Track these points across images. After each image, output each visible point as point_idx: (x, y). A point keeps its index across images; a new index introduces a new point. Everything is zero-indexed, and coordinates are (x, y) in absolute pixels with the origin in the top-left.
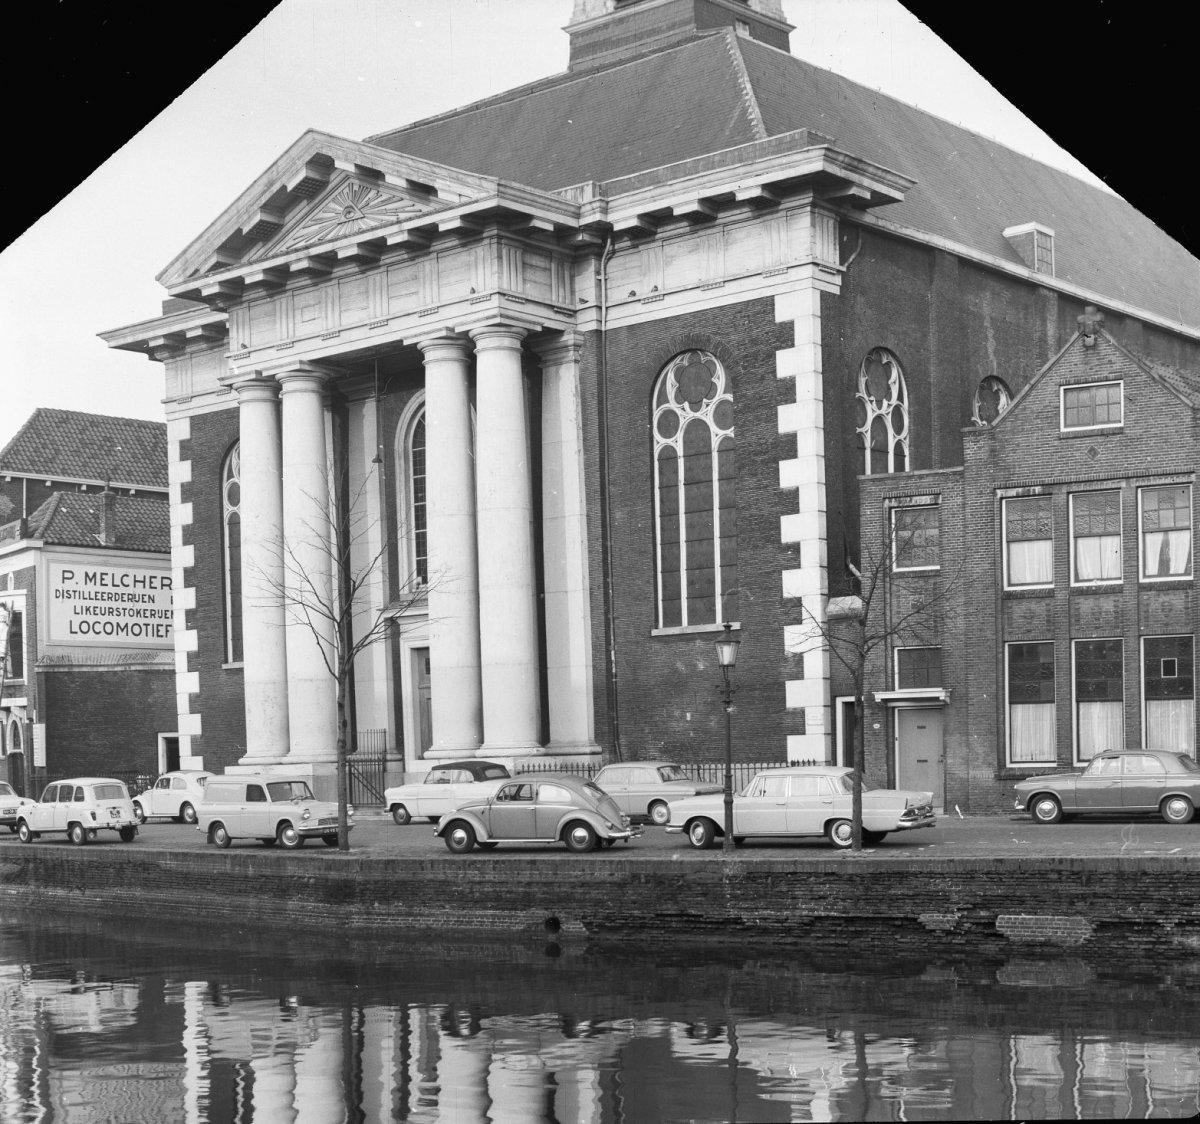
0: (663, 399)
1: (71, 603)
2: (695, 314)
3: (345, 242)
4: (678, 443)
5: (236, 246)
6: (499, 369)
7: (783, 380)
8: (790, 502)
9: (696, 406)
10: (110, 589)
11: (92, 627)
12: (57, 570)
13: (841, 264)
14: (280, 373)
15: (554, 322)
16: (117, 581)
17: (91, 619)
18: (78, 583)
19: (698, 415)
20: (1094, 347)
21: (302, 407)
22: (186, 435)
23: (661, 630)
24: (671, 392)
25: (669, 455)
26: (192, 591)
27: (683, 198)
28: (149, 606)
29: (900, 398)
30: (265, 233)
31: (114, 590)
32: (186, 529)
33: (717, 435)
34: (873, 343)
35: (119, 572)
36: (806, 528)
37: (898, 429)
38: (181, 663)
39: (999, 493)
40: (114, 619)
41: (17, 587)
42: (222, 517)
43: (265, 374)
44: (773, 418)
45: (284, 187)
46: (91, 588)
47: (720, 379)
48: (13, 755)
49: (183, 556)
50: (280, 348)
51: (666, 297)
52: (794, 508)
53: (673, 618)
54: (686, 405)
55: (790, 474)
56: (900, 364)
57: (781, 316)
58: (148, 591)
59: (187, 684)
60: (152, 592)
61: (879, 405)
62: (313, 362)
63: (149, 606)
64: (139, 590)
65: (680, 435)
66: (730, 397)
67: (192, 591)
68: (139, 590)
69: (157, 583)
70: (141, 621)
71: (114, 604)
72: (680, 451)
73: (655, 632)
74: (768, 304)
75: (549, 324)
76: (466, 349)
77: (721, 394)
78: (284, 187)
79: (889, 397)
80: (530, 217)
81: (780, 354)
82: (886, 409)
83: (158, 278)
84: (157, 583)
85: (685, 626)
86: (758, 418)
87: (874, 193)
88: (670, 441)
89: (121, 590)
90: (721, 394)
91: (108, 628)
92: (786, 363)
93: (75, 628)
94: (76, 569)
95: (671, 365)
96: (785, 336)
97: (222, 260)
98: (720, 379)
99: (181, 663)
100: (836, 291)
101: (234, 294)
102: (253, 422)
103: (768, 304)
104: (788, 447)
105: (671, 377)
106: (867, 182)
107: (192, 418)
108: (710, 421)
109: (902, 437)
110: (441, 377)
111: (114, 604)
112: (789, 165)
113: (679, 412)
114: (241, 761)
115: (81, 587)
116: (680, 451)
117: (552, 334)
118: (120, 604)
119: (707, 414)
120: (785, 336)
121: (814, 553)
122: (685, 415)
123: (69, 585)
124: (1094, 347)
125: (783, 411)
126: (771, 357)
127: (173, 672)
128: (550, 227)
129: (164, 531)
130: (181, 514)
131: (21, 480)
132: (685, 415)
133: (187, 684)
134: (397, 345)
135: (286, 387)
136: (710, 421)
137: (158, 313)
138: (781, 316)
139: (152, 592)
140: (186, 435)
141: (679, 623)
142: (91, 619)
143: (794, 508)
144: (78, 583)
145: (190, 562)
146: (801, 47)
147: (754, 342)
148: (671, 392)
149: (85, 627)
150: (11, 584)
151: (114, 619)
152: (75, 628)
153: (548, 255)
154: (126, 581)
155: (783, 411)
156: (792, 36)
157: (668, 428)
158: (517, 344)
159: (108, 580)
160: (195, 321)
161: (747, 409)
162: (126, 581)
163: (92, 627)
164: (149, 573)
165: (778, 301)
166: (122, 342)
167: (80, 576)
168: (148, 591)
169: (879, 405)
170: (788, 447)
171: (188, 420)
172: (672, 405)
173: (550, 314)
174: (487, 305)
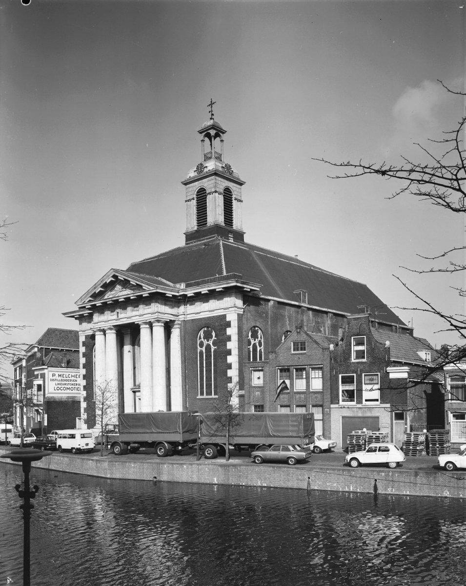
0: (200, 338)
1: (55, 382)
2: (208, 317)
3: (121, 297)
4: (204, 349)
5: (95, 296)
6: (159, 331)
7: (228, 335)
8: (230, 366)
9: (208, 341)
10: (65, 378)
11: (60, 389)
12: (51, 374)
13: (243, 306)
14: (105, 328)
15: (173, 318)
16: (67, 376)
17: (60, 386)
18: (57, 377)
19: (208, 343)
20: (299, 332)
21: (112, 336)
22: (84, 340)
23: (199, 397)
24: (202, 337)
25: (201, 353)
26: (85, 380)
27: (204, 290)
28: (76, 383)
29: (261, 338)
30: (101, 294)
31: (66, 379)
32: (83, 364)
33: (213, 348)
34: (253, 324)
35: (67, 374)
36: (233, 373)
37: (260, 346)
38: (82, 400)
39: (277, 368)
40: (66, 386)
41: (41, 378)
42: (11, 464)
43: (102, 328)
44: (226, 345)
45: (106, 282)
46: (60, 378)
47: (214, 334)
48: (39, 421)
49: (83, 371)
50: (105, 322)
51: (367, 166)
52: (230, 368)
53: (202, 394)
54: (206, 340)
55: (230, 359)
56: (261, 330)
57: (228, 319)
58: (75, 379)
59: (83, 405)
60: (76, 379)
61: (255, 341)
62: (113, 326)
63: (76, 383)
64: (73, 378)
65: (204, 348)
66: (216, 338)
67: (85, 380)
68: (73, 378)
69: (78, 376)
70: (73, 386)
71: (66, 382)
72: (204, 352)
73: (197, 397)
74: (224, 316)
75: (171, 319)
76: (151, 325)
77: (214, 338)
78: (106, 282)
79: (258, 338)
80: (166, 294)
81: (227, 329)
82: (257, 341)
83: (75, 303)
84: (78, 376)
85: (205, 396)
86: (222, 345)
87: (251, 289)
88: (202, 349)
89: (68, 378)
90: (214, 338)
91: (64, 389)
92: (229, 331)
93: (56, 389)
94: (57, 374)
95: (203, 329)
96: (228, 324)
97: (91, 299)
98: (214, 334)
99: (82, 400)
100: (242, 313)
101: (94, 308)
102: (99, 338)
103: (224, 316)
104: (229, 353)
105: (202, 333)
106: (248, 287)
107: (86, 336)
108: (211, 344)
109: (261, 348)
110: (144, 332)
111: (66, 382)
112: (228, 283)
113: (204, 342)
114: (94, 427)
115: (57, 378)
116: (204, 352)
117: (172, 322)
118: (68, 382)
119: (211, 342)
120: (228, 324)
121: (235, 379)
122: (205, 342)
123: (54, 378)
124: (299, 332)
125: (228, 343)
126: (225, 330)
127: (80, 402)
128: (171, 296)
129: (79, 364)
130: (83, 360)
131: (43, 348)
132: (205, 342)
133: (83, 405)
134: (133, 323)
135: (107, 332)
136: (211, 344)
137: (77, 309)
138: (228, 319)
139: (76, 379)
140: (84, 340)
141: (211, 395)
142: (60, 386)
143: (230, 368)
144: (57, 377)
145: (85, 373)
146: (247, 239)
147: (221, 325)
148: (202, 337)
149: (58, 389)
150: (39, 377)
151: (66, 386)
152: (56, 389)
153: (172, 301)
154: (69, 376)
155: (228, 343)
156: (245, 235)
157: (201, 345)
158: (163, 325)
159: (64, 376)
160: (86, 312)
161: (219, 342)
162: (69, 376)
163: (60, 389)
164: (75, 374)
165: (227, 315)
166: (68, 315)
167: (57, 375)
168: (75, 379)
169: (255, 341)
170: (229, 353)
171: (84, 336)
172: (202, 340)
173: (172, 316)
174: (155, 315)
